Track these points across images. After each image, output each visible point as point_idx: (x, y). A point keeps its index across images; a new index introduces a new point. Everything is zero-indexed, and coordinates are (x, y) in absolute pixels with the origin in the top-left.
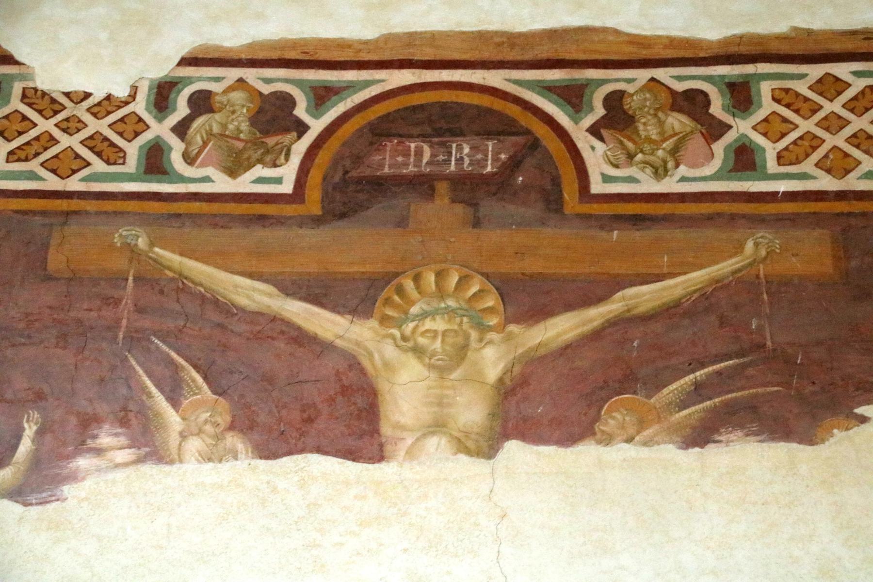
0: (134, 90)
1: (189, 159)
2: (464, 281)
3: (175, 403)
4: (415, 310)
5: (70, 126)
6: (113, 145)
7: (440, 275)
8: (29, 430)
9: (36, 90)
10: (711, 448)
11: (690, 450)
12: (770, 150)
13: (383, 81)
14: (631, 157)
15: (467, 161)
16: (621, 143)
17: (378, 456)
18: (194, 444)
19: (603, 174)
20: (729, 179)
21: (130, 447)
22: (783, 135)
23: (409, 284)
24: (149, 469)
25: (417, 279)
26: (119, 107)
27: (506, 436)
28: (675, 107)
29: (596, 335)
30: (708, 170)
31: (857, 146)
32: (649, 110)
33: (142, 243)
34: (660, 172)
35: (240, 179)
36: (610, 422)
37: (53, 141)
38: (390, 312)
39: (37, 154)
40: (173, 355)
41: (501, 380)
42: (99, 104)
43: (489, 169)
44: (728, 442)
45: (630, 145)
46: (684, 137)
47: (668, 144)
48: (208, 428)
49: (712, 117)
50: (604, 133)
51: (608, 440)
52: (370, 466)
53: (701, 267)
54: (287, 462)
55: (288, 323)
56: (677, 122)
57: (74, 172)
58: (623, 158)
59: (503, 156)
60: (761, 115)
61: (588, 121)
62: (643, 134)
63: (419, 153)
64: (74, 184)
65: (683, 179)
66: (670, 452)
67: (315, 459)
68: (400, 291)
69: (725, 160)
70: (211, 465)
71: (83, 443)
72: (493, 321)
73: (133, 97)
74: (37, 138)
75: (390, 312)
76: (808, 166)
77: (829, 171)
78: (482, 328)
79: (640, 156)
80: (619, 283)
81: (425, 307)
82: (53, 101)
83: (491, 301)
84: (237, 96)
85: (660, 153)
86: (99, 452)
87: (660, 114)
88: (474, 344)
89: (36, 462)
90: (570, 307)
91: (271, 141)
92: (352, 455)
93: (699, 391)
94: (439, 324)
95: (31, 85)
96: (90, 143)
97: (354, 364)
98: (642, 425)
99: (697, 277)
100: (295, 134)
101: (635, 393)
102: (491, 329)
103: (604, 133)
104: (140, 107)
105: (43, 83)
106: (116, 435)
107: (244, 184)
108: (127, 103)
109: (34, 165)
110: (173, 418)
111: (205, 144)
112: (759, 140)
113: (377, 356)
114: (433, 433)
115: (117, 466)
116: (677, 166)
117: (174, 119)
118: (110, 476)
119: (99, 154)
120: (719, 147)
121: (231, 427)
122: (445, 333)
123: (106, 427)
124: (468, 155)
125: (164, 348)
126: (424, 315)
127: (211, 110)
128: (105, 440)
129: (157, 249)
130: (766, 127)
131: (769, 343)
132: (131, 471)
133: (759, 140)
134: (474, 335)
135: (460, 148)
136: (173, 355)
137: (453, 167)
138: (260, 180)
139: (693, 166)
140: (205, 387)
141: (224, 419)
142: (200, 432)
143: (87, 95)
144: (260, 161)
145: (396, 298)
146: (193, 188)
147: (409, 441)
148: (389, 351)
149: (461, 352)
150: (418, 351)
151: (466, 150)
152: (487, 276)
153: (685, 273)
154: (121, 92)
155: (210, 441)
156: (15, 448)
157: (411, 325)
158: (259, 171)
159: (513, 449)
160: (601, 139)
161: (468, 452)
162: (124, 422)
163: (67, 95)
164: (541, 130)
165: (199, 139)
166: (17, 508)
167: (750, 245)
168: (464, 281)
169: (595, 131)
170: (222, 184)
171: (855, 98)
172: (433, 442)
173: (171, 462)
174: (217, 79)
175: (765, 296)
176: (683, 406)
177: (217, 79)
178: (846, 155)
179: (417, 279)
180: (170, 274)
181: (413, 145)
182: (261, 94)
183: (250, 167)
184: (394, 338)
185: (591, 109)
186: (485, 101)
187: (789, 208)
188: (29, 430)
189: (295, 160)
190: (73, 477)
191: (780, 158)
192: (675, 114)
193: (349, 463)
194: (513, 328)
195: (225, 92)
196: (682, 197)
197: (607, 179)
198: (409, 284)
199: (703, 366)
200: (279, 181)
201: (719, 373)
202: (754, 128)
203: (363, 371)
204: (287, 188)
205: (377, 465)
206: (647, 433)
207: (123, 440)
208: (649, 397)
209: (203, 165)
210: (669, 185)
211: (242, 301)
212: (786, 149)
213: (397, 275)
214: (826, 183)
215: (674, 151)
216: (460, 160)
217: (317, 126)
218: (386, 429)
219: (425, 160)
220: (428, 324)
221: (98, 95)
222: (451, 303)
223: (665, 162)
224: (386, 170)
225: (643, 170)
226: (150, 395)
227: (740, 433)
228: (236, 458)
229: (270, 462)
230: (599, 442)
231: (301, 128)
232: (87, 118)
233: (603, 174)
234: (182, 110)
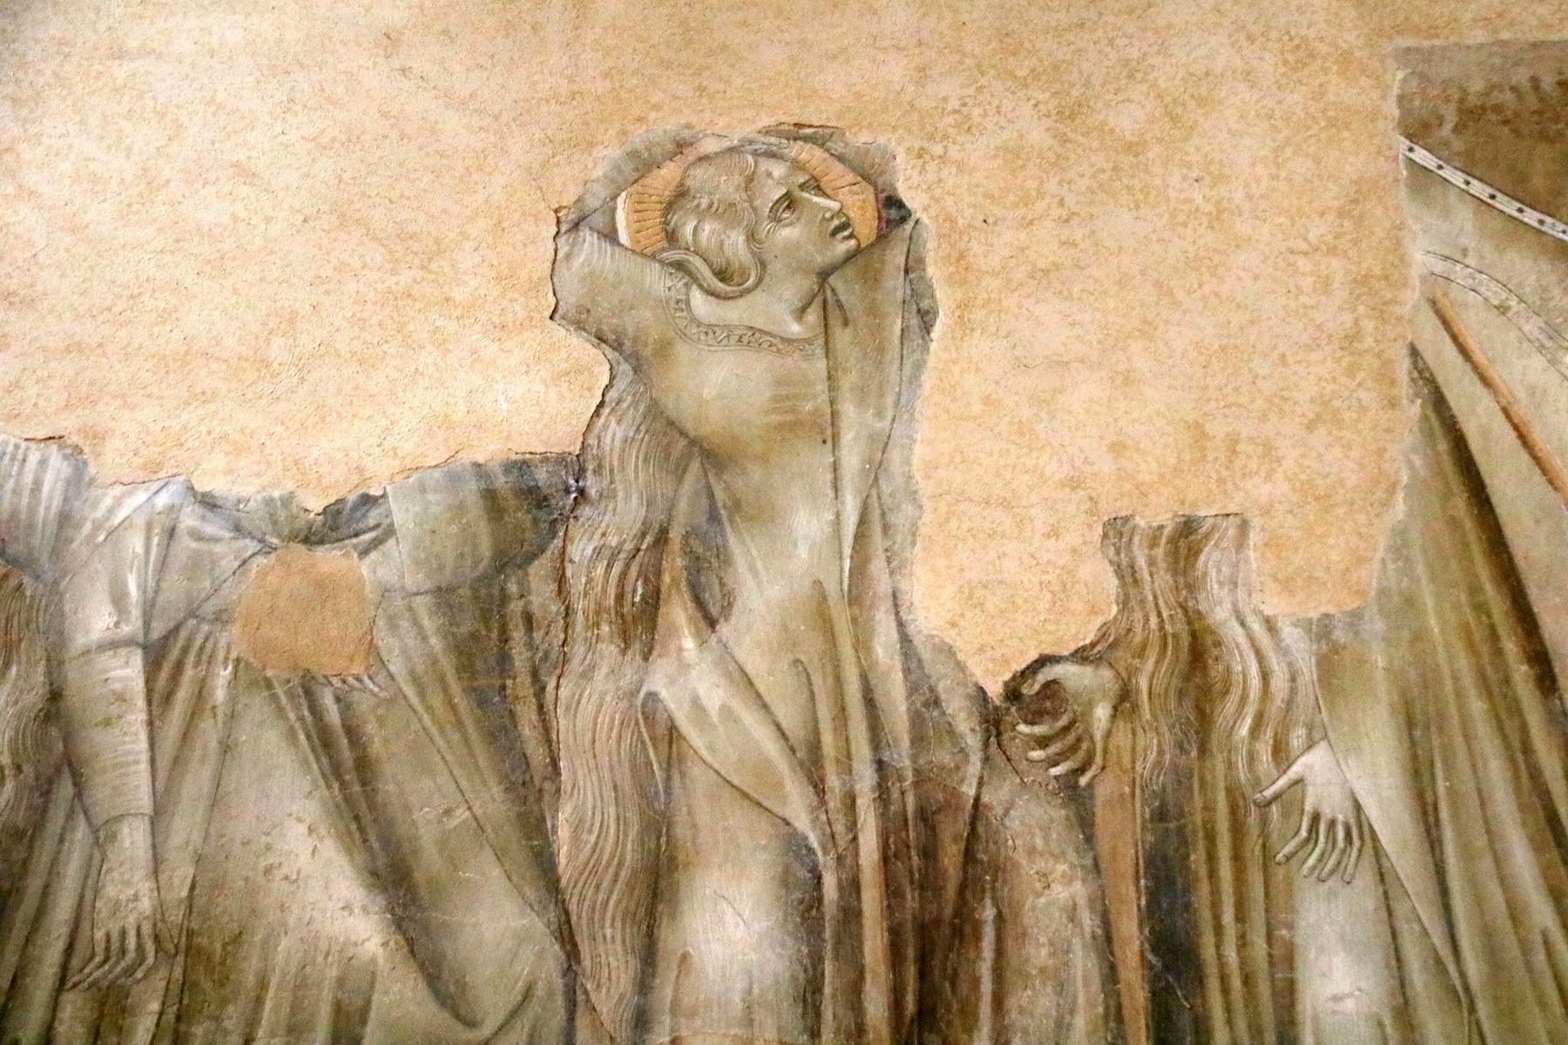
90: (1546, 872)
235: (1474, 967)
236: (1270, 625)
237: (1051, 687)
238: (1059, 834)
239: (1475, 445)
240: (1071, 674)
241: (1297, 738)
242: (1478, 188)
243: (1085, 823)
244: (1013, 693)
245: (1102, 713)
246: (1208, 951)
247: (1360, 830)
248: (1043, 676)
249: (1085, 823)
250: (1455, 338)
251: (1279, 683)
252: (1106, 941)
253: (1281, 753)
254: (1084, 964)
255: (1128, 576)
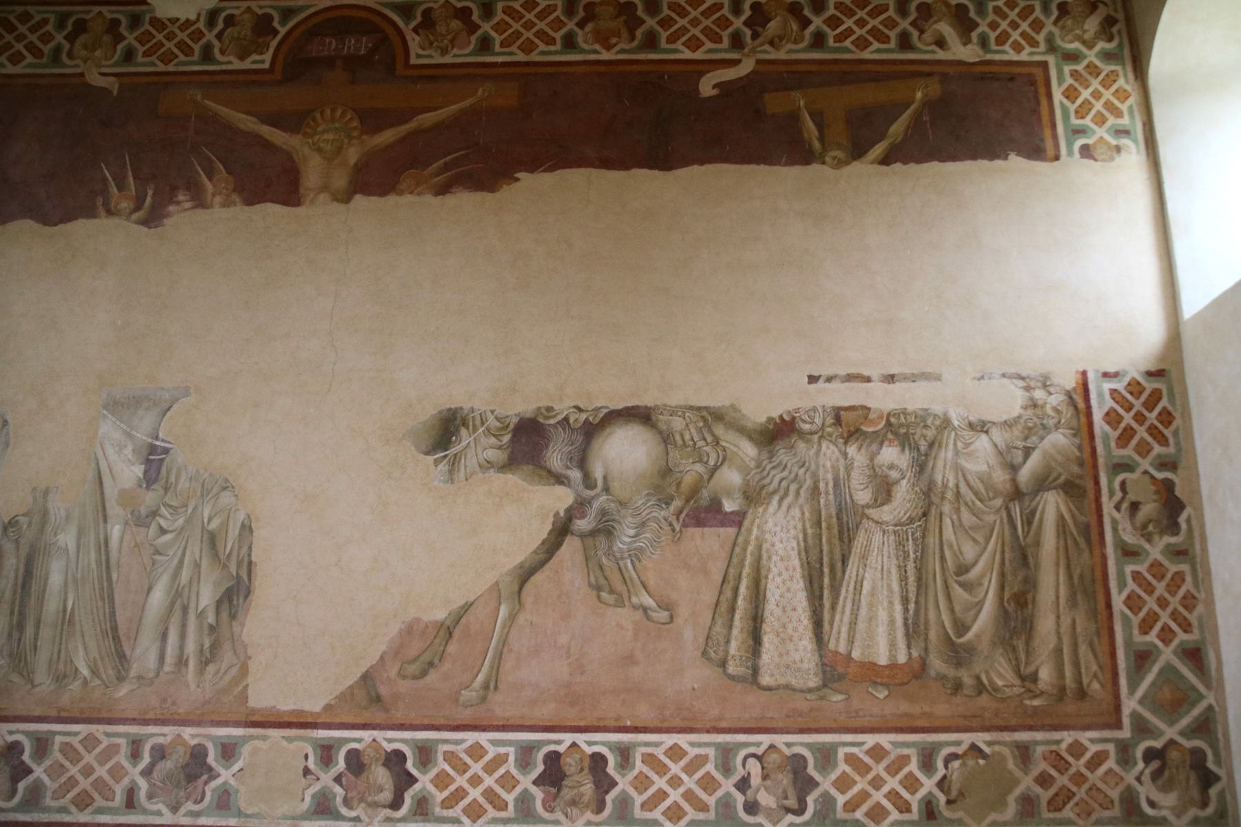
0: (199, 15)
1: (222, 52)
2: (343, 114)
3: (210, 179)
4: (320, 129)
5: (170, 36)
6: (188, 46)
7: (333, 111)
8: (150, 193)
9: (155, 18)
10: (448, 196)
11: (439, 197)
12: (498, 39)
13: (315, 5)
14: (431, 44)
15: (352, 48)
16: (428, 36)
17: (174, 814)
18: (218, 199)
19: (417, 54)
20: (478, 55)
21: (191, 201)
22: (505, 31)
23: (318, 116)
24: (199, 211)
25: (322, 113)
26: (192, 25)
27: (355, 192)
28: (456, 17)
29: (403, 140)
30: (467, 51)
31: (538, 38)
32: (354, 137)
33: (199, 98)
34: (444, 52)
35: (245, 62)
36: (403, 186)
37: (163, 45)
38: (309, 131)
39: (155, 52)
40: (211, 155)
41: (356, 164)
42: (183, 24)
43: (362, 52)
44: (455, 193)
45: (432, 38)
46: (457, 34)
47: (449, 37)
48: (224, 191)
49: (473, 21)
50: (420, 31)
51: (401, 193)
52: (294, 208)
53: (455, 103)
54: (258, 206)
55: (261, 137)
56: (456, 24)
57: (171, 61)
58: (427, 44)
59: (370, 45)
60: (496, 20)
61: (413, 24)
62: (439, 31)
63: (330, 43)
64: (171, 68)
65: (455, 56)
66: (429, 198)
67: (270, 205)
68: (314, 120)
69: (476, 44)
70: (224, 209)
71: (172, 198)
72: (355, 134)
73: (198, 19)
74: (155, 44)
75: (309, 131)
76: (514, 48)
77: (523, 51)
78: (350, 137)
79: (435, 44)
80: (416, 112)
81: (325, 128)
82: (163, 23)
83: (355, 123)
84: (247, 16)
85: (445, 41)
86: (178, 203)
87: (448, 21)
88: (345, 146)
89: (153, 208)
90: (391, 126)
91: (261, 40)
92: (286, 203)
93: (446, 168)
94: (331, 136)
95: (153, 15)
96: (178, 45)
97: (289, 157)
98: (418, 185)
99: (454, 108)
100: (272, 36)
101: (417, 169)
102: (354, 137)
103: (420, 31)
104: (201, 25)
105: (159, 14)
106: (186, 195)
107: (247, 65)
108: (195, 23)
109: (153, 58)
110: (209, 186)
111: (230, 43)
112: (493, 34)
113: (300, 153)
114: (322, 192)
115: (186, 210)
116: (453, 48)
117: (216, 31)
118: (182, 215)
119: (182, 51)
120: (473, 38)
121: (234, 190)
122: (333, 140)
123: (181, 190)
124: (353, 45)
125: (206, 151)
126: (323, 132)
127: (234, 25)
128: (181, 198)
129: (207, 102)
130: (496, 28)
131: (481, 142)
132: (189, 212)
133: (493, 34)
134: (346, 141)
135: (350, 41)
136: (211, 155)
137: (345, 52)
138: (255, 62)
139: (461, 48)
140: (224, 171)
141: (231, 187)
142: (220, 193)
143: (178, 19)
144: (255, 52)
145: (312, 123)
146: (224, 67)
147: (312, 196)
148: (306, 150)
149: (339, 150)
150: (319, 150)
151: (353, 42)
152: (355, 110)
153: (447, 106)
154: (193, 17)
155: (225, 197)
156: (145, 200)
157: (318, 137)
158: (255, 57)
159: (359, 199)
160: (417, 33)
161: (337, 200)
162: (188, 189)
163: (169, 20)
164: (390, 31)
165: (227, 41)
166: (145, 229)
167: (480, 92)
168: (343, 114)
169: (415, 30)
170: (237, 65)
171: (541, 12)
172: (322, 197)
173: (207, 208)
174: (238, 8)
175: (484, 118)
176: (437, 175)
177: (238, 8)
178: (533, 42)
179: (322, 113)
180: (210, 113)
181: (327, 40)
182: (257, 14)
183: (250, 55)
184: (308, 143)
185: (415, 18)
186: (363, 14)
187: (502, 70)
188: (150, 193)
189: (271, 50)
190: (168, 215)
191: (502, 45)
192: (455, 20)
193: (285, 207)
194: (365, 137)
195: (241, 15)
196: (453, 66)
197: (418, 56)
198: (318, 116)
199: (450, 154)
200: (263, 62)
201: (457, 158)
202: (492, 28)
203: (293, 161)
204: (266, 66)
205: (297, 208)
206: (419, 189)
207: (188, 198)
208: (423, 171)
209: (228, 55)
210: (448, 59)
211: (242, 127)
212: (505, 39)
213: (313, 111)
214: (521, 57)
215: (452, 41)
216: (349, 48)
217: (283, 31)
218: (302, 191)
219: (333, 47)
220: (326, 136)
221: (183, 19)
222: (337, 125)
223: (448, 46)
224: (314, 54)
225: (436, 51)
226: (200, 175)
227: (461, 188)
228: (235, 205)
229: (250, 207)
230: (397, 194)
231: (276, 32)
232: (177, 32)
233: (417, 54)
234: (220, 25)
235: (79, 575)
236: (59, 509)
237: (17, 522)
238: (917, 514)
239: (102, 472)
240: (21, 519)
241: (59, 532)
242: (114, 419)
243: (18, 549)
244: (10, 522)
245: (25, 526)
246: (34, 573)
247: (67, 549)
248: (16, 519)
249: (18, 549)
250: (102, 493)
251: (58, 521)
252: (17, 570)
253: (56, 534)
254: (12, 575)
255: (35, 499)
